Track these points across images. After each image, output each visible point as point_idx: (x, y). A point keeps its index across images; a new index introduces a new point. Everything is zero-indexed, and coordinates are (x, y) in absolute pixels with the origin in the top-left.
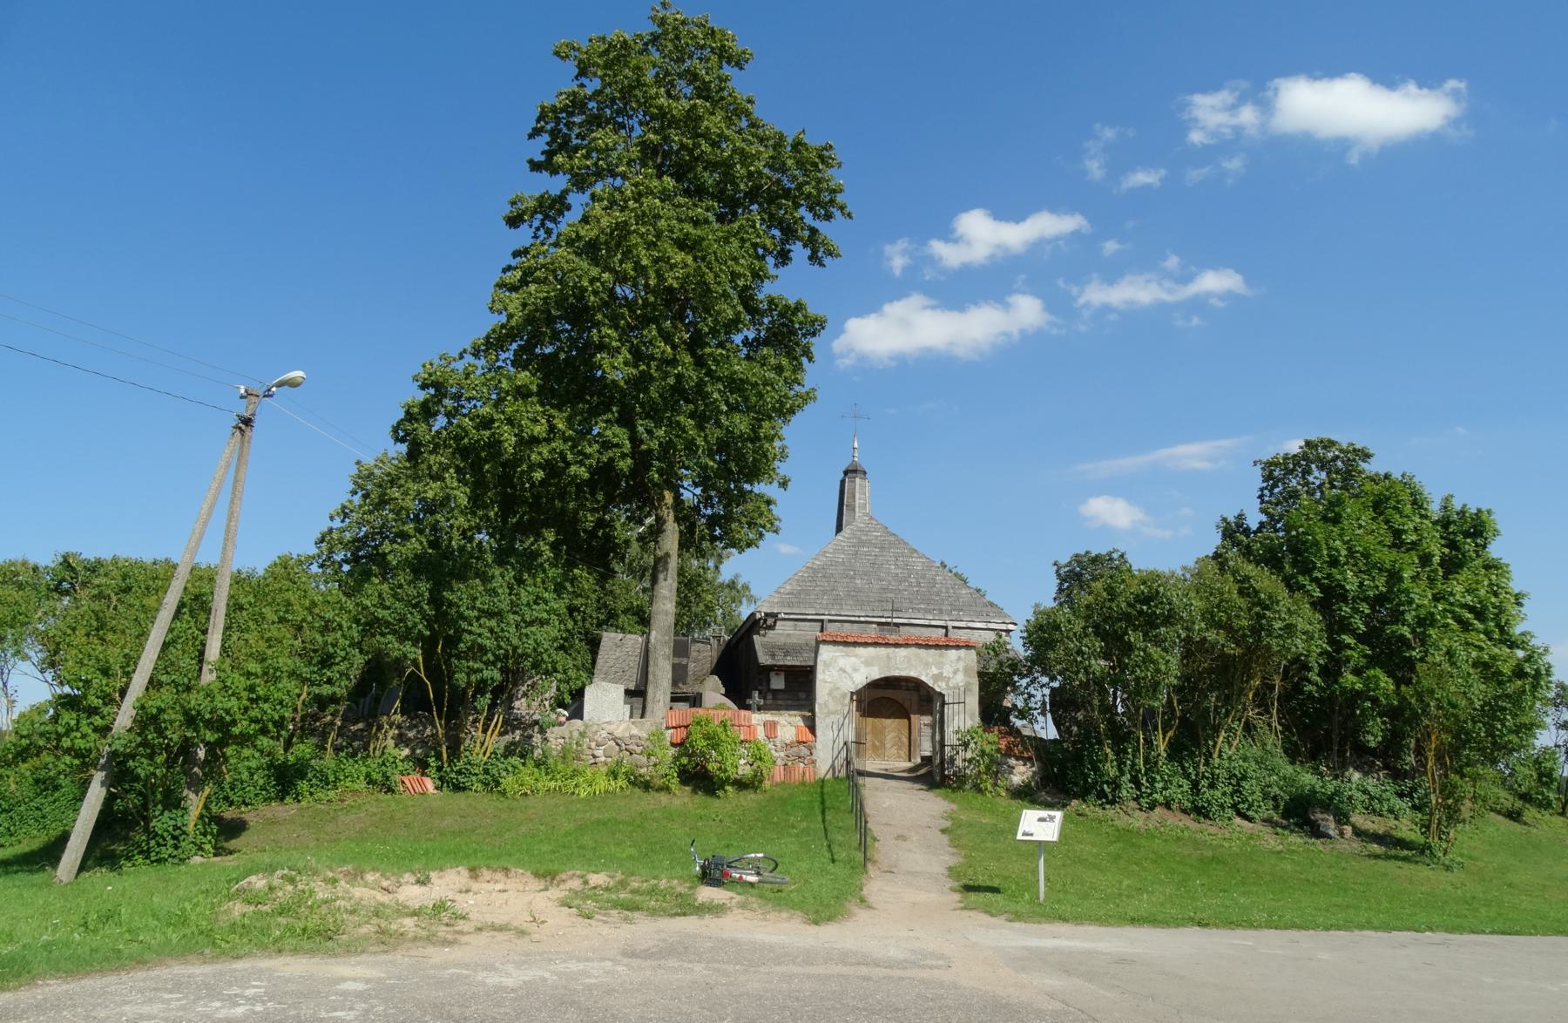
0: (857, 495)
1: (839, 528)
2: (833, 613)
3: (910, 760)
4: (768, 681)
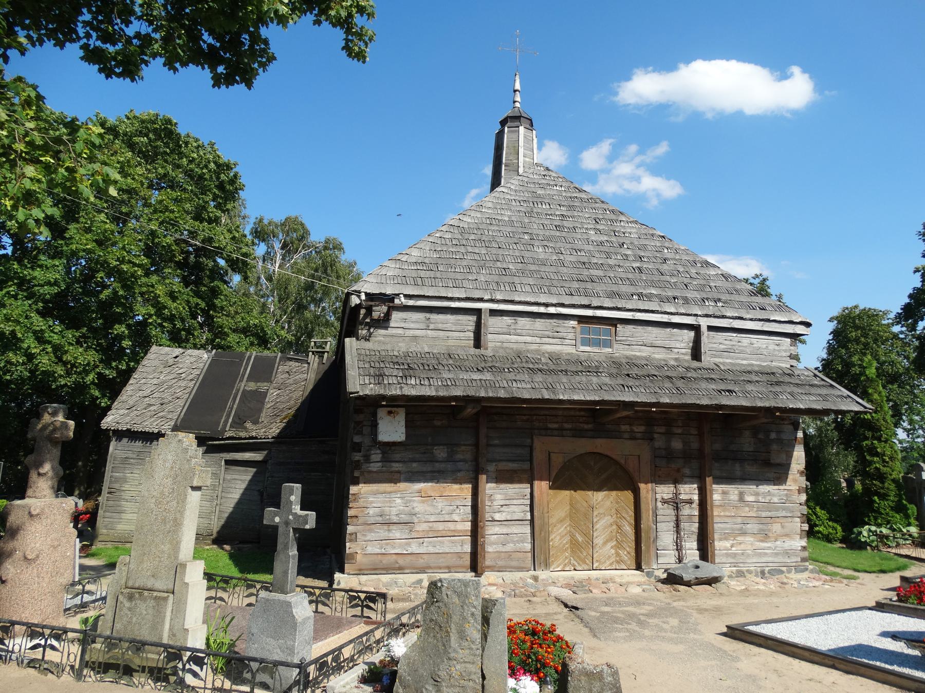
0: (521, 151)
1: (496, 182)
2: (499, 297)
3: (639, 567)
4: (374, 426)
